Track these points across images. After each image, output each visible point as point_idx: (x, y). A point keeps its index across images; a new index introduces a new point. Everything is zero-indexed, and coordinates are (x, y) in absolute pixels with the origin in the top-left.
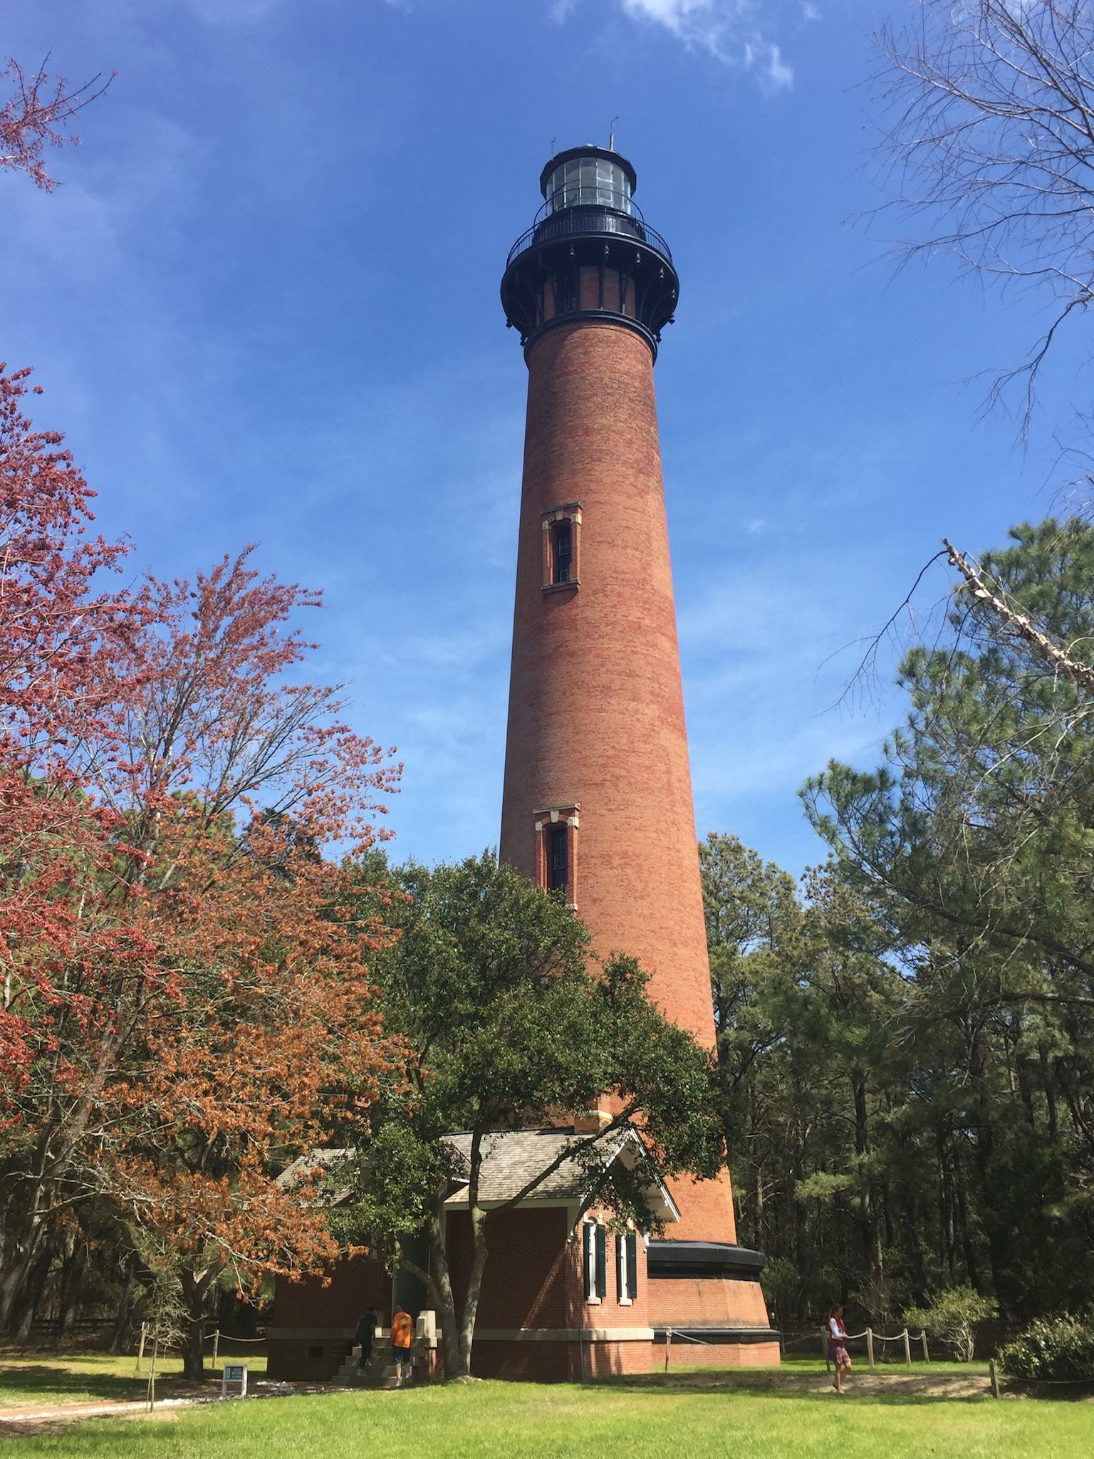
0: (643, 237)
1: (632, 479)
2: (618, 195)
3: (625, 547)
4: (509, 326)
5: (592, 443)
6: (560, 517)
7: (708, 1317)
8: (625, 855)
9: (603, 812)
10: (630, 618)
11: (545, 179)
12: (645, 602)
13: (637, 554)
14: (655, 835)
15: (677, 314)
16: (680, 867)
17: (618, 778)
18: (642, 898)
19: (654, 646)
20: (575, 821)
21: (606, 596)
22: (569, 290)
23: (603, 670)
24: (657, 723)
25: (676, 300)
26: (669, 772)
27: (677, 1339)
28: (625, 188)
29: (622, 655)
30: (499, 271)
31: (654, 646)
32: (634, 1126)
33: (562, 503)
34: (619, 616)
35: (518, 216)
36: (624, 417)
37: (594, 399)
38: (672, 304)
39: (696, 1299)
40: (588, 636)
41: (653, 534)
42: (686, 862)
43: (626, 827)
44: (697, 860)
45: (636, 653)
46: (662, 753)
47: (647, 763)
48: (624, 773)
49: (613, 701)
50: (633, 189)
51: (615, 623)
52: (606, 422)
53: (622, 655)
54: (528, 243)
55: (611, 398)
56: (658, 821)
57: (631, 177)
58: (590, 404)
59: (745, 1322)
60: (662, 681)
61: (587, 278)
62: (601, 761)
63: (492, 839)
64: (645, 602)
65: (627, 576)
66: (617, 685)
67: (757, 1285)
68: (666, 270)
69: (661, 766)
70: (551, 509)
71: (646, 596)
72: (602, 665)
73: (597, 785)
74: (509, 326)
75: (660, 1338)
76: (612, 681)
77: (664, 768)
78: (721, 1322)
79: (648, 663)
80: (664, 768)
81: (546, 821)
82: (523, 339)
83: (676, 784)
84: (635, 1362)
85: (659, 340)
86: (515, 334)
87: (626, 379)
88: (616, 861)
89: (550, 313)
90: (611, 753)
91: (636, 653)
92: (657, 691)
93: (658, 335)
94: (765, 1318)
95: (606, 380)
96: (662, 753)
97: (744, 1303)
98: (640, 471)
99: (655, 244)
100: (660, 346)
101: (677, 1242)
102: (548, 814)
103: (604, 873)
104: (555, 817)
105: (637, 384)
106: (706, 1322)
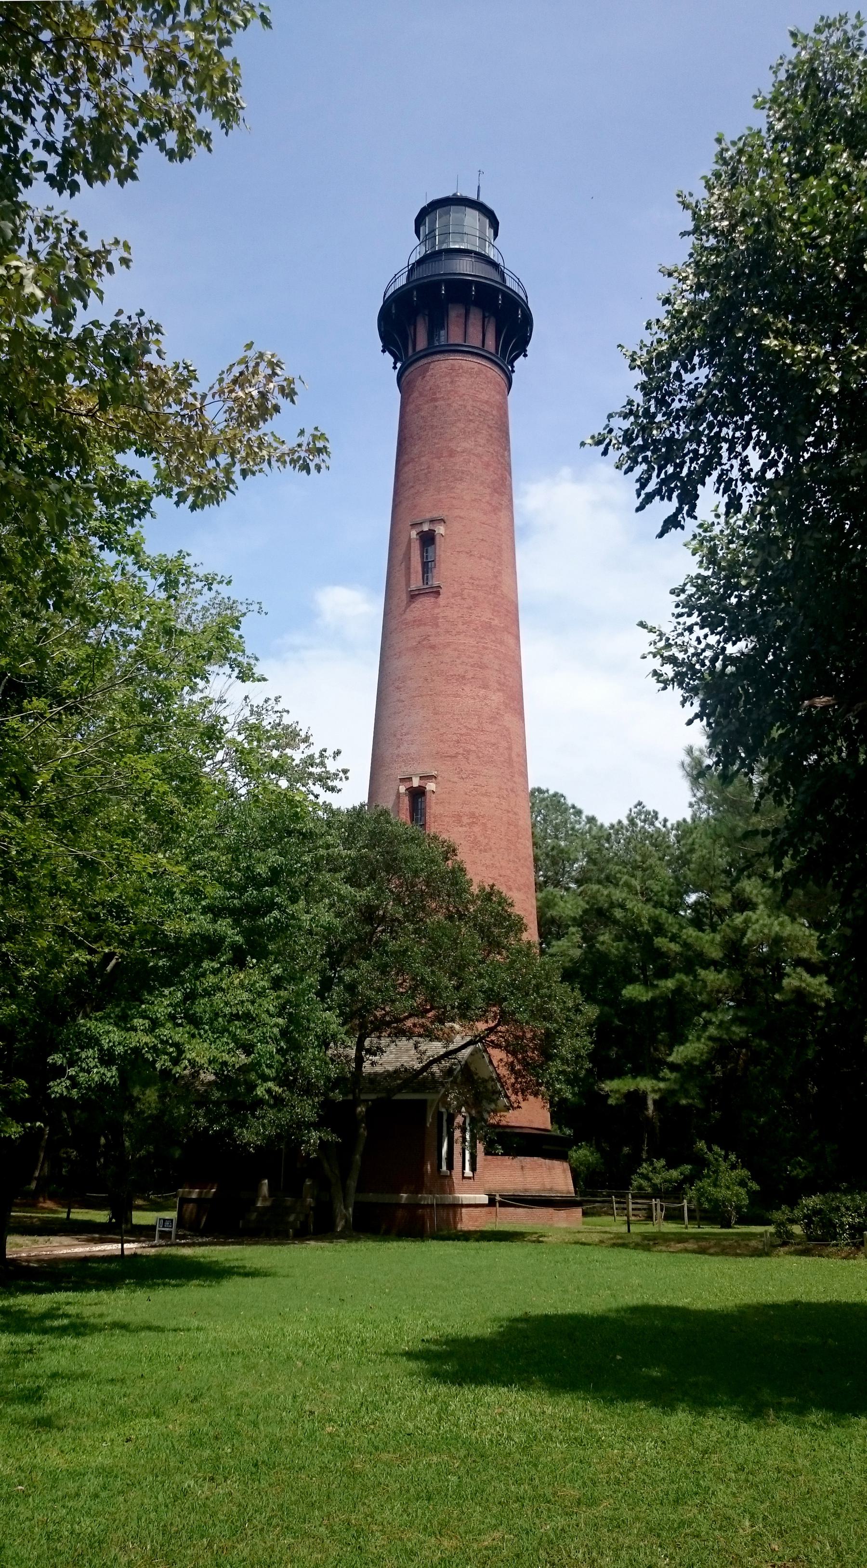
0: (504, 280)
1: (488, 498)
2: (483, 239)
3: (480, 558)
4: (383, 351)
5: (455, 464)
6: (426, 528)
7: (528, 1186)
8: (472, 815)
9: (456, 779)
10: (483, 619)
11: (419, 221)
12: (495, 605)
13: (491, 564)
14: (497, 800)
15: (529, 348)
16: (516, 826)
17: (469, 752)
18: (485, 851)
19: (502, 643)
20: (431, 786)
21: (464, 599)
22: (437, 324)
23: (459, 661)
24: (502, 707)
25: (530, 337)
26: (510, 748)
27: (503, 1204)
28: (489, 232)
29: (475, 649)
30: (533, 307)
31: (502, 643)
32: (107, 1058)
33: (428, 516)
34: (473, 617)
35: (395, 253)
36: (482, 442)
37: (458, 424)
38: (526, 340)
39: (519, 1173)
40: (448, 632)
41: (504, 546)
42: (521, 823)
43: (474, 792)
44: (529, 844)
45: (486, 648)
46: (505, 733)
47: (493, 741)
48: (474, 748)
49: (467, 689)
50: (496, 234)
51: (471, 622)
52: (467, 446)
53: (475, 649)
54: (402, 281)
55: (472, 425)
56: (500, 789)
57: (494, 224)
58: (454, 429)
59: (557, 1192)
60: (507, 673)
61: (455, 313)
62: (455, 738)
63: (365, 799)
64: (495, 605)
65: (482, 583)
66: (470, 675)
67: (566, 1165)
68: (505, 295)
69: (504, 744)
70: (418, 520)
71: (496, 600)
72: (458, 658)
73: (451, 757)
74: (383, 351)
75: (492, 1202)
76: (466, 671)
77: (506, 745)
78: (539, 1191)
79: (496, 657)
80: (506, 745)
81: (408, 785)
82: (395, 363)
83: (515, 758)
84: (468, 1221)
85: (513, 371)
86: (389, 358)
87: (486, 408)
88: (465, 820)
89: (422, 343)
90: (464, 731)
91: (486, 648)
92: (503, 680)
93: (513, 367)
94: (572, 1188)
95: (469, 408)
96: (505, 733)
97: (556, 1177)
98: (495, 491)
99: (515, 288)
100: (514, 376)
101: (686, 1251)
102: (410, 779)
103: (456, 829)
104: (416, 783)
105: (494, 412)
106: (526, 1190)
